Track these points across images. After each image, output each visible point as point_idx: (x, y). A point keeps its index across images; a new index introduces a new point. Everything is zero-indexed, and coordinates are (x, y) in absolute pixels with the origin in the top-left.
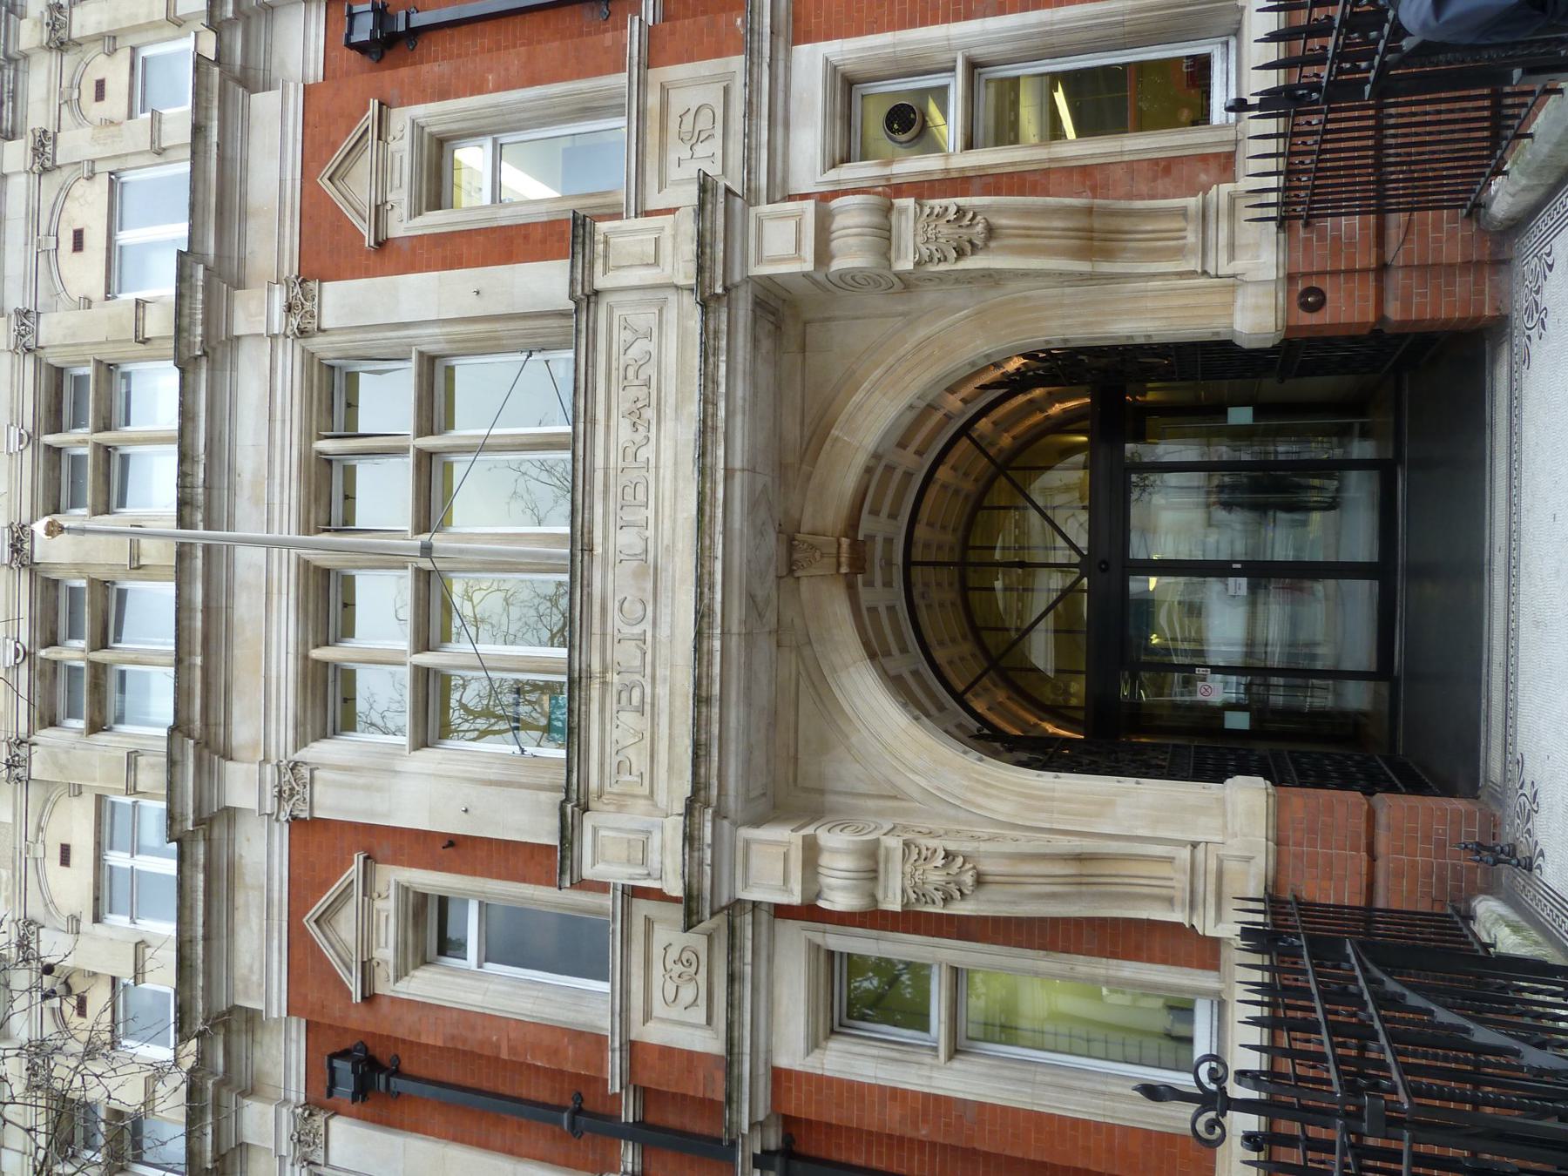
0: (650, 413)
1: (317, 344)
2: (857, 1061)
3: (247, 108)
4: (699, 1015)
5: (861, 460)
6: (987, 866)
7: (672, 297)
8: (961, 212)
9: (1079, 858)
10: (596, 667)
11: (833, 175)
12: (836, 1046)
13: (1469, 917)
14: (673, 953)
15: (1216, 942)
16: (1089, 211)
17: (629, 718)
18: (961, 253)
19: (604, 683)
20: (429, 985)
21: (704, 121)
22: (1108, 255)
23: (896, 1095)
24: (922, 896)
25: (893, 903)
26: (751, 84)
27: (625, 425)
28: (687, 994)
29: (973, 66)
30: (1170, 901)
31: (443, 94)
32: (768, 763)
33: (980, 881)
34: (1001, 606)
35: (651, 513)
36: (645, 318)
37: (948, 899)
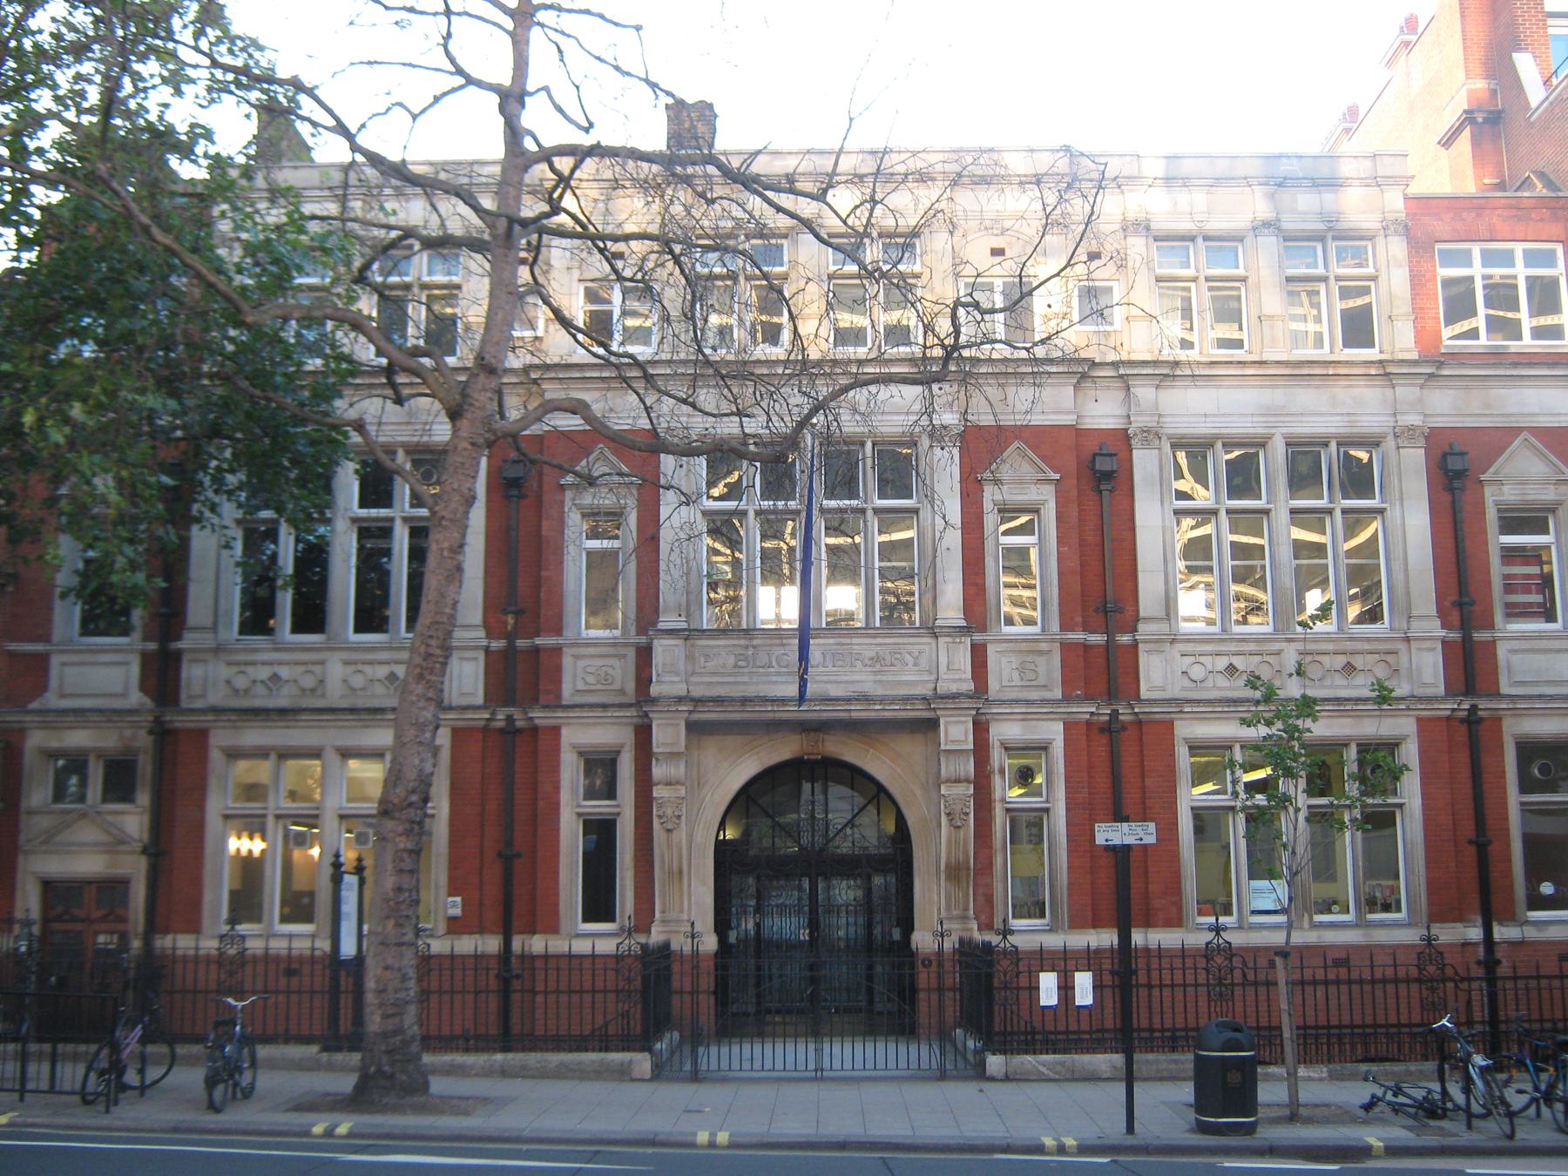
0: (878, 667)
1: (925, 442)
2: (570, 773)
3: (1065, 385)
4: (580, 686)
5: (858, 763)
6: (675, 834)
7: (933, 677)
8: (967, 814)
9: (681, 872)
10: (755, 642)
11: (997, 744)
12: (575, 756)
13: (671, 1030)
14: (610, 671)
15: (649, 932)
16: (968, 868)
17: (731, 660)
18: (948, 814)
19: (747, 647)
20: (575, 523)
21: (1031, 675)
22: (948, 878)
23: (557, 789)
24: (660, 806)
25: (657, 792)
26: (1044, 702)
27: (872, 654)
28: (591, 679)
29: (1047, 810)
30: (663, 912)
31: (1060, 518)
32: (711, 724)
33: (669, 831)
34: (484, 462)
35: (831, 669)
36: (924, 662)
37: (660, 817)
